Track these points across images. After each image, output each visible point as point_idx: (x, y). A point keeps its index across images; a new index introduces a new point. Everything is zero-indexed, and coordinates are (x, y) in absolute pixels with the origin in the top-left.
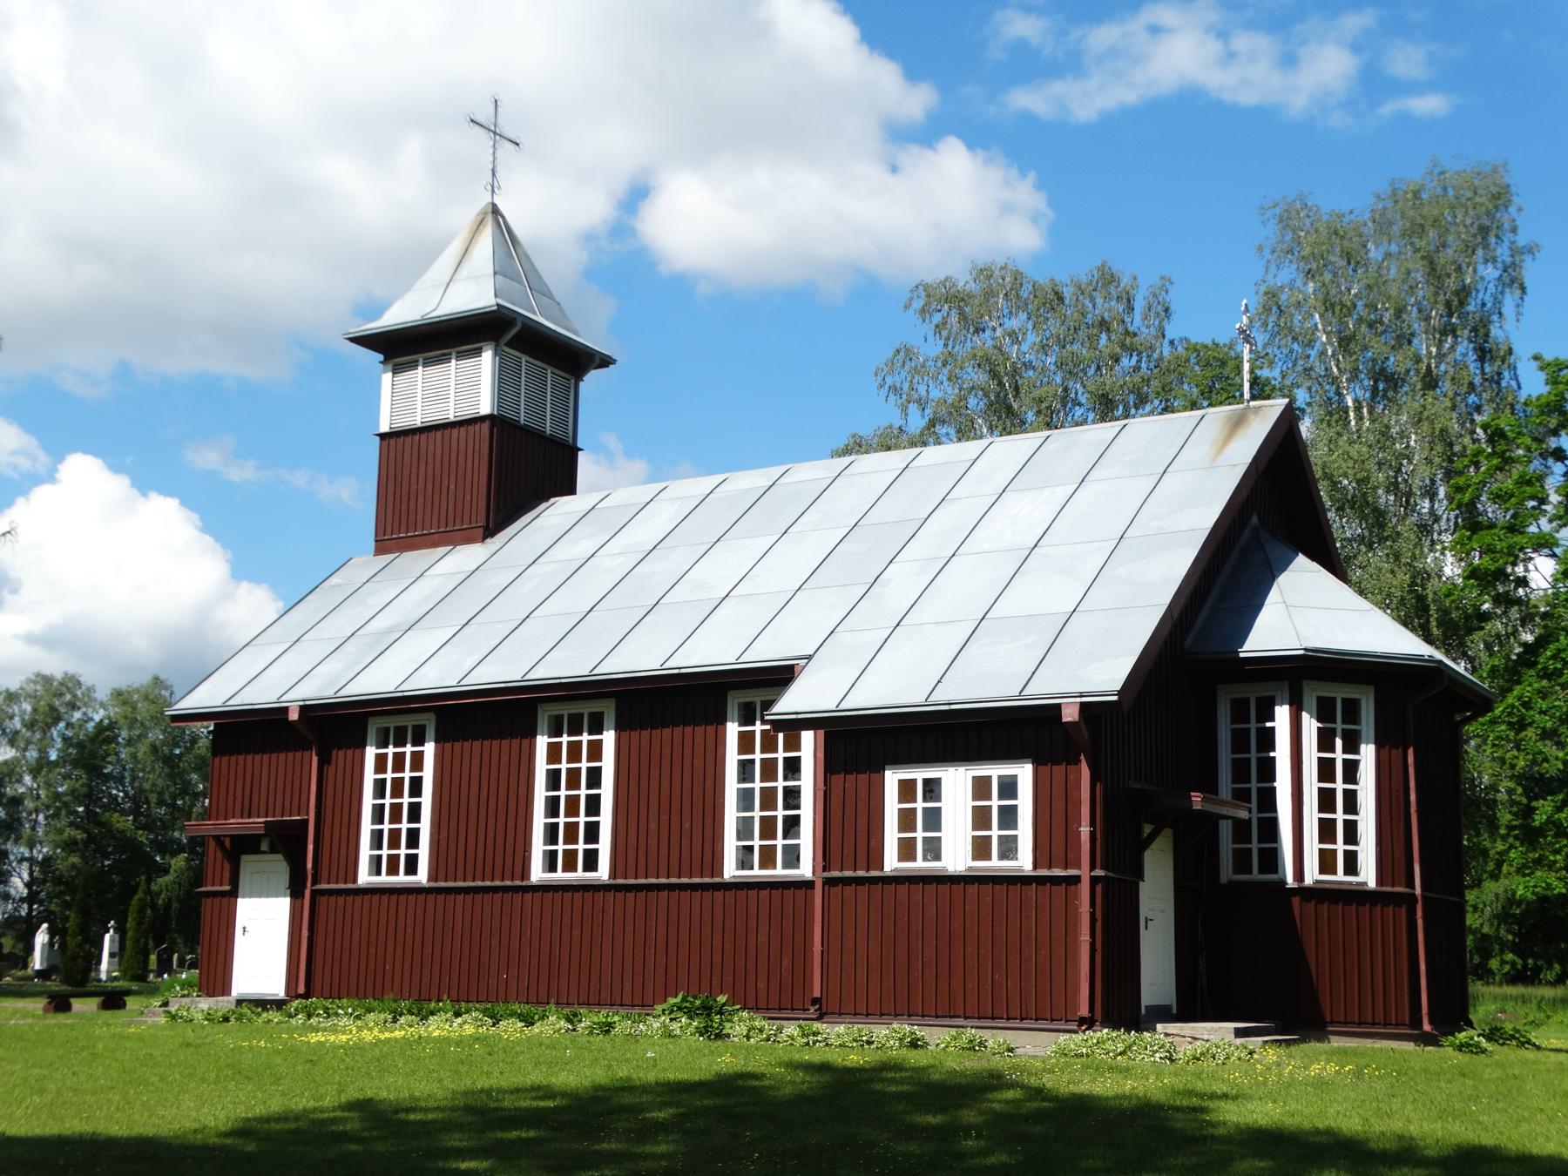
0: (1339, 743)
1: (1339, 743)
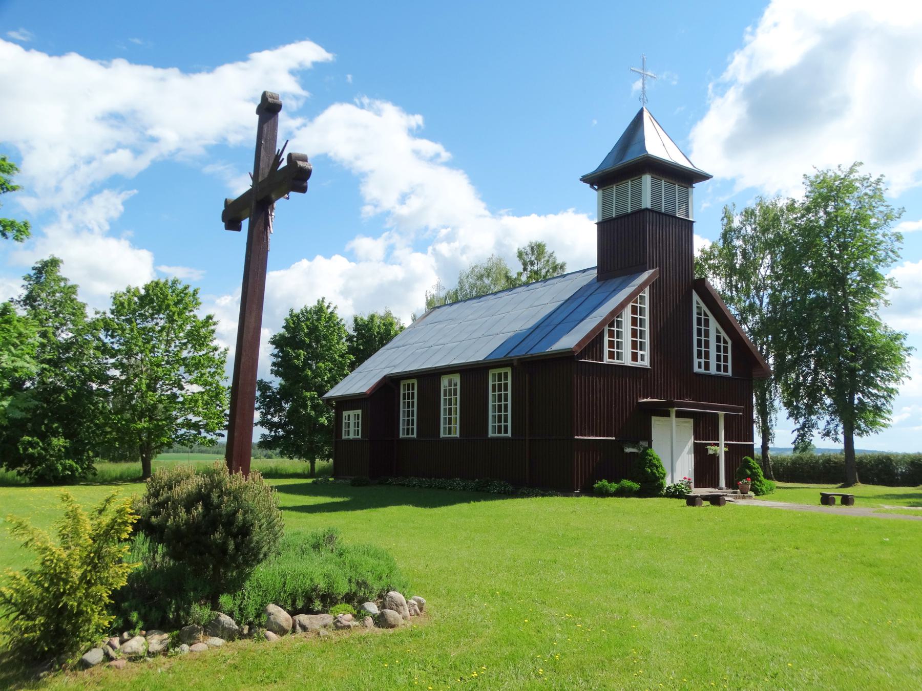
0: (612, 329)
1: (612, 329)
